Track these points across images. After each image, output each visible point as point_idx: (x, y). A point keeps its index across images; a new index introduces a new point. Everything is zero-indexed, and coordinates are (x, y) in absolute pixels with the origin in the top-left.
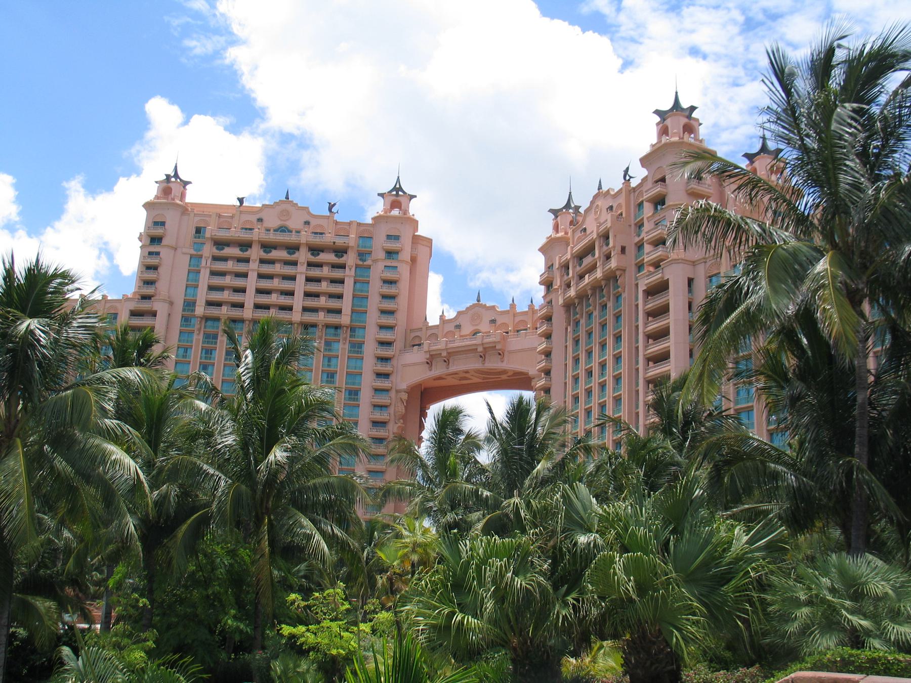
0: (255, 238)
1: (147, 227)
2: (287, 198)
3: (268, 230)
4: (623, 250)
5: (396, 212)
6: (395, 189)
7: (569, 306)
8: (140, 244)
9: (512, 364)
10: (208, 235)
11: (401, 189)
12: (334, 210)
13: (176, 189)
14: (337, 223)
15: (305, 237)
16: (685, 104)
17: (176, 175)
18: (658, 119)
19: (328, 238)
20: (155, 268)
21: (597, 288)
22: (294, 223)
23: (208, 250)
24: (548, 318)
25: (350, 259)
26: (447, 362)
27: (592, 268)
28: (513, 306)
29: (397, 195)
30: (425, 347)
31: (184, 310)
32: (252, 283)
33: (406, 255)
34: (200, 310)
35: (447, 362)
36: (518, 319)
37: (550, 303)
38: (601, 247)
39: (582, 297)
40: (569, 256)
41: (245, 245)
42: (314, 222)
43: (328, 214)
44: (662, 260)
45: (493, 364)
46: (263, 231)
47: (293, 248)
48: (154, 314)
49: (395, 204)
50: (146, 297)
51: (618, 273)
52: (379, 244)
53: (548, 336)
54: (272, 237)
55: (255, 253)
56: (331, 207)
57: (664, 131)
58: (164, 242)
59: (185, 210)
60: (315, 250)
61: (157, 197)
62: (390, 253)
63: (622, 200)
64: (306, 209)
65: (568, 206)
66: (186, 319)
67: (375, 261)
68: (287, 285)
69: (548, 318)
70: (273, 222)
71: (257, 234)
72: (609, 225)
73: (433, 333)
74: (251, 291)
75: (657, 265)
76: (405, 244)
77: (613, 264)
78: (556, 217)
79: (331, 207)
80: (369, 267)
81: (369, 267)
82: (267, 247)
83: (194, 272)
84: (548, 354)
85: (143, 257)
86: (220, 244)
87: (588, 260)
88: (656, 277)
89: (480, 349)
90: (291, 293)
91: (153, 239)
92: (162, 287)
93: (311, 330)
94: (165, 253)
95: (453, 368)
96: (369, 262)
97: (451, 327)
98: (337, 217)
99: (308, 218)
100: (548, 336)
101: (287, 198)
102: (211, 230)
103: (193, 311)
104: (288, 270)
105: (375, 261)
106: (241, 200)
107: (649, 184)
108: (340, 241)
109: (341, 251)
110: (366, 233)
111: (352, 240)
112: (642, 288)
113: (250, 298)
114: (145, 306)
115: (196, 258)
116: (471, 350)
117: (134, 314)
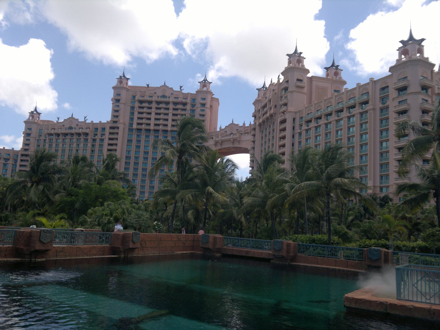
0: (154, 100)
1: (114, 96)
2: (165, 84)
3: (158, 97)
4: (276, 106)
5: (205, 89)
6: (204, 80)
7: (260, 125)
8: (112, 102)
9: (243, 145)
10: (136, 99)
11: (206, 80)
12: (182, 89)
13: (124, 81)
14: (183, 93)
15: (172, 99)
16: (299, 51)
17: (124, 76)
18: (288, 58)
19: (180, 100)
20: (117, 111)
21: (267, 119)
22: (167, 94)
23: (137, 105)
24: (254, 129)
25: (188, 107)
26: (233, 143)
27: (266, 113)
28: (244, 124)
29: (205, 82)
30: (214, 139)
31: (129, 126)
32: (153, 116)
33: (208, 106)
34: (135, 126)
35: (221, 144)
36: (245, 129)
37: (255, 123)
38: (269, 105)
39: (264, 122)
40: (260, 108)
41: (150, 102)
42: (174, 93)
43: (180, 90)
44: (285, 111)
45: (237, 145)
46: (156, 97)
47: (167, 103)
48: (118, 128)
49: (204, 86)
50: (115, 122)
51: (273, 115)
52: (199, 101)
53: (254, 135)
54: (160, 99)
55: (154, 105)
56: (181, 87)
57: (290, 62)
58: (121, 102)
59: (128, 89)
60: (175, 104)
61: (117, 84)
62: (203, 105)
63: (277, 87)
64: (172, 89)
65: (333, 65)
66: (131, 130)
67: (197, 108)
68: (166, 117)
69: (254, 129)
70: (160, 93)
71: (154, 99)
72: (271, 97)
73: (217, 134)
74: (153, 119)
75: (283, 113)
76: (208, 102)
77: (272, 111)
78: (328, 71)
79: (181, 87)
80: (195, 110)
81: (195, 110)
82: (158, 103)
83: (132, 113)
84: (254, 142)
85: (113, 107)
86: (141, 102)
87: (265, 109)
88: (283, 118)
89: (232, 140)
90: (167, 120)
91: (117, 101)
92: (121, 119)
93: (386, 90)
94: (122, 106)
95: (224, 146)
96: (195, 108)
97: (223, 132)
98: (183, 91)
99: (172, 92)
100: (254, 135)
101: (165, 84)
102: (138, 97)
103: (132, 126)
104: (166, 112)
105: (197, 108)
106: (148, 85)
107: (284, 83)
108: (184, 101)
109: (185, 104)
110: (194, 97)
111: (189, 100)
112: (279, 121)
113: (152, 122)
114: (114, 125)
115: (133, 108)
116: (229, 140)
117: (111, 128)
